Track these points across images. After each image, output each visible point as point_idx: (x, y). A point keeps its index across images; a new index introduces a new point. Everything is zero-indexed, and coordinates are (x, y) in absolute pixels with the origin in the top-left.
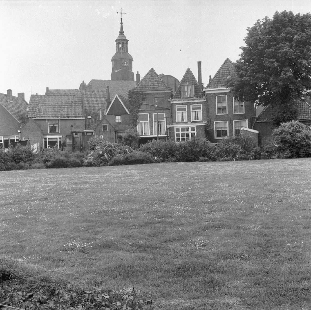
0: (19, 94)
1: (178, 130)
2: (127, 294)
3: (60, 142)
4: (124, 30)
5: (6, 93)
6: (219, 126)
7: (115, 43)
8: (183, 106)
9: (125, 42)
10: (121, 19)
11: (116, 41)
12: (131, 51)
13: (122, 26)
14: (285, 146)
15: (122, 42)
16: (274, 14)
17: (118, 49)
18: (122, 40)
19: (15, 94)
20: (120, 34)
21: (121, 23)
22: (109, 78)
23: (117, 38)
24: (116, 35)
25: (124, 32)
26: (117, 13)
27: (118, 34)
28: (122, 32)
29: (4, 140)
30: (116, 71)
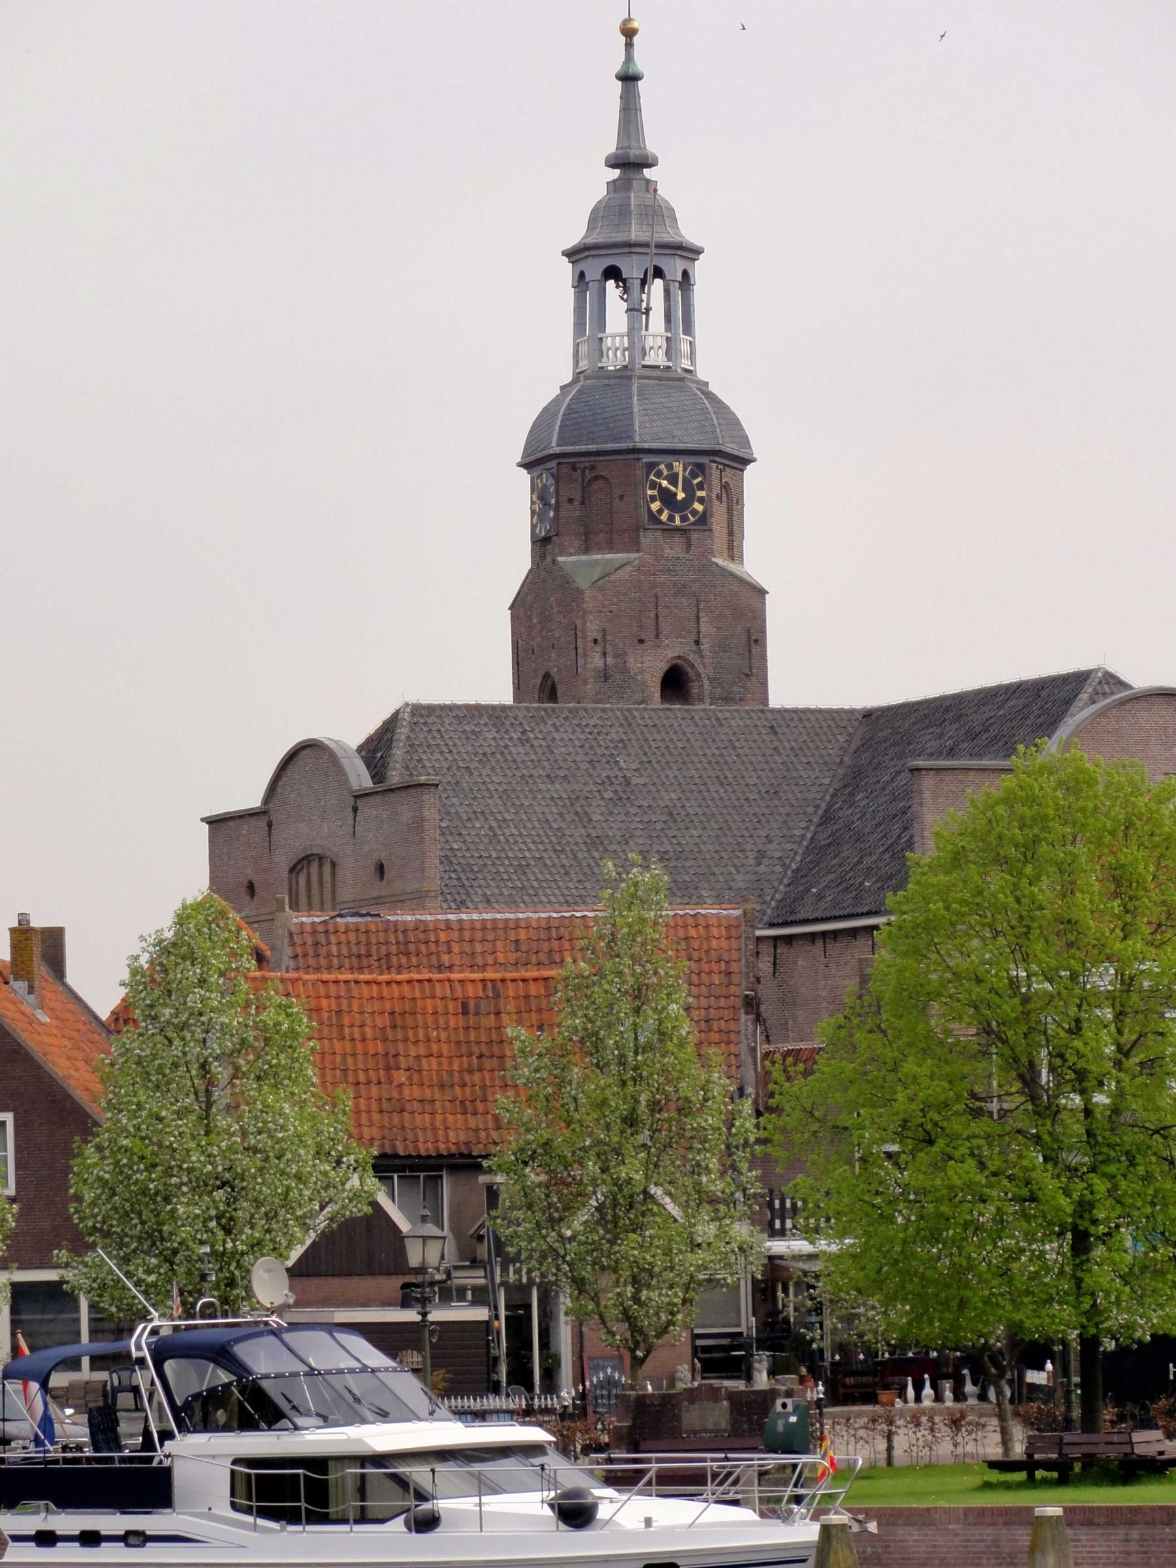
4: (653, 142)
7: (566, 270)
8: (924, 1494)
10: (629, 33)
21: (629, 79)
25: (647, 162)
28: (630, 164)
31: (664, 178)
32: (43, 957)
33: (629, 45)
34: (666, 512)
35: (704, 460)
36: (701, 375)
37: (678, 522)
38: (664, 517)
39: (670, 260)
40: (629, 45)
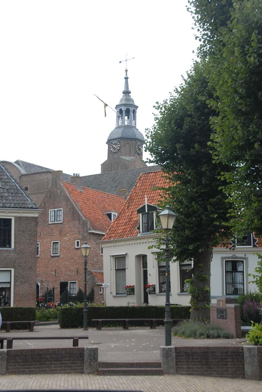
2: (238, 100)
4: (130, 89)
10: (126, 71)
11: (117, 107)
13: (127, 83)
14: (170, 357)
16: (137, 113)
21: (126, 78)
23: (118, 103)
26: (120, 62)
27: (121, 95)
28: (127, 93)
31: (132, 96)
32: (39, 286)
33: (126, 73)
34: (112, 149)
35: (119, 140)
36: (137, 128)
37: (115, 151)
38: (113, 151)
39: (131, 107)
40: (126, 73)
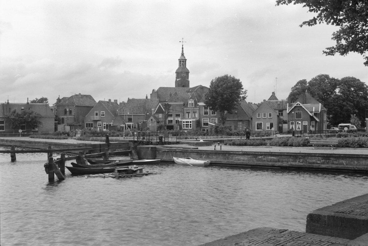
0: (115, 100)
1: (184, 122)
3: (132, 126)
4: (184, 53)
5: (108, 101)
6: (205, 121)
7: (178, 61)
9: (184, 61)
10: (183, 45)
11: (179, 60)
12: (188, 66)
15: (183, 62)
17: (180, 65)
18: (182, 59)
19: (112, 101)
20: (181, 56)
21: (183, 48)
22: (173, 85)
24: (179, 56)
28: (183, 54)
29: (106, 125)
30: (178, 80)
